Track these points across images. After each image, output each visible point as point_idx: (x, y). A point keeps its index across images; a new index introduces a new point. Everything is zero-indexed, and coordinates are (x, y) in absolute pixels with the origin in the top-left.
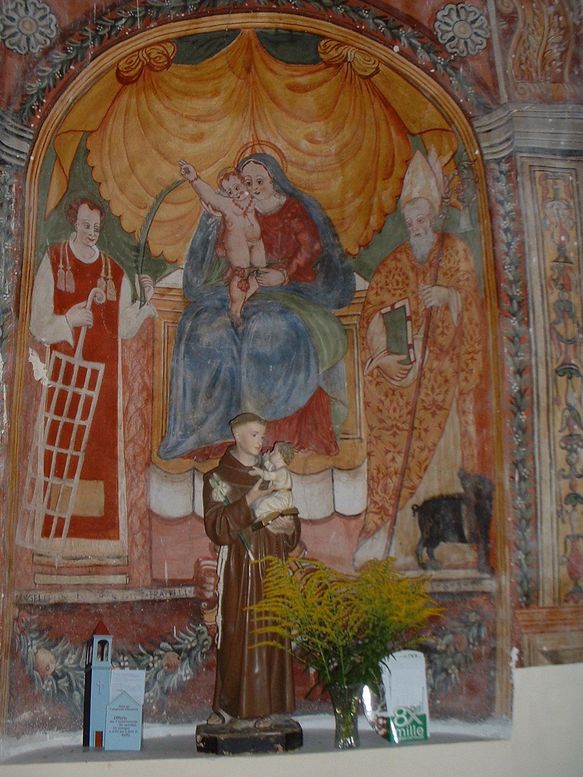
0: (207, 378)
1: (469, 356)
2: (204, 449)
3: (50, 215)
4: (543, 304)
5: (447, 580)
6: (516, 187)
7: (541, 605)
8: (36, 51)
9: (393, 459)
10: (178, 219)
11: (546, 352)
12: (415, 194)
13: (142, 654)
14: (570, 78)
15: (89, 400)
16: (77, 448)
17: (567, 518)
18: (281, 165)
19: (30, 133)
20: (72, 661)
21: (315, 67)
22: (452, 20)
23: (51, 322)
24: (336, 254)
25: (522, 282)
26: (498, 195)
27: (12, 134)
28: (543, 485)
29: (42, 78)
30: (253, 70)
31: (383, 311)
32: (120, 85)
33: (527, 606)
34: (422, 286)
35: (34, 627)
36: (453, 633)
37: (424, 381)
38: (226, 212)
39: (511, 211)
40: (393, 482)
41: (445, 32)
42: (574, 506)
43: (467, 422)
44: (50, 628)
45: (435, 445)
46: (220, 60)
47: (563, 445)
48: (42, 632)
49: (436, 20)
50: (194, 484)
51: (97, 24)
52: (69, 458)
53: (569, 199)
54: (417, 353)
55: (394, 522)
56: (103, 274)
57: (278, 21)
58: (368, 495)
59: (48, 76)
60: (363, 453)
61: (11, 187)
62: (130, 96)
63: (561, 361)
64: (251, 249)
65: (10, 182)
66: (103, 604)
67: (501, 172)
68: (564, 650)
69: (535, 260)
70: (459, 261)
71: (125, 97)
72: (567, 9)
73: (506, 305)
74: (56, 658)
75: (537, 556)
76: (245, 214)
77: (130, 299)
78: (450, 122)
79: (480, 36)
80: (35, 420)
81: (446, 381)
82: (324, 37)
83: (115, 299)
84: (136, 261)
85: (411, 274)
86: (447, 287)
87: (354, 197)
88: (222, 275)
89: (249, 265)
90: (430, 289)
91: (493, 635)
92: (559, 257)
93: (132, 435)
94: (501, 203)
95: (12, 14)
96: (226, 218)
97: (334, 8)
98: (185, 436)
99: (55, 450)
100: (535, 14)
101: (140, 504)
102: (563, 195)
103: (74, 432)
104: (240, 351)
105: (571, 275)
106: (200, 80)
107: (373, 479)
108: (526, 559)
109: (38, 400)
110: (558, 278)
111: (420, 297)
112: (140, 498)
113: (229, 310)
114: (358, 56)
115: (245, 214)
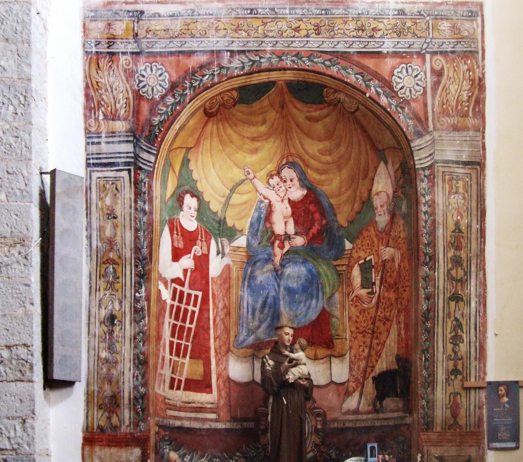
0: (260, 301)
1: (402, 289)
2: (259, 343)
3: (168, 201)
4: (444, 259)
5: (389, 419)
6: (433, 186)
7: (435, 430)
8: (157, 97)
9: (363, 351)
10: (242, 204)
11: (444, 287)
12: (380, 189)
13: (226, 458)
14: (473, 114)
15: (193, 312)
16: (187, 341)
17: (451, 383)
18: (304, 169)
19: (155, 150)
20: (188, 460)
21: (322, 106)
22: (403, 74)
23: (171, 266)
24: (336, 225)
25: (432, 244)
26: (422, 190)
27: (145, 150)
28: (439, 364)
29: (161, 115)
30: (285, 108)
31: (360, 262)
32: (206, 118)
33: (427, 430)
34: (381, 247)
35: (167, 438)
36: (391, 448)
37: (381, 304)
38: (271, 199)
39: (429, 200)
40: (362, 364)
41: (398, 83)
42: (456, 376)
43: (400, 328)
44: (176, 440)
45: (385, 342)
46: (265, 101)
47: (451, 341)
48: (171, 442)
49: (393, 75)
50: (253, 364)
51: (192, 79)
52: (183, 346)
53: (465, 193)
54: (376, 289)
55: (363, 387)
56: (199, 238)
57: (298, 76)
58: (350, 371)
59: (164, 113)
60: (347, 347)
61: (145, 183)
62: (213, 125)
63: (452, 292)
64: (286, 223)
65: (145, 180)
66: (204, 429)
67: (425, 176)
68: (446, 456)
69: (441, 231)
70: (400, 232)
71: (210, 125)
72: (475, 67)
73: (422, 258)
74: (180, 457)
75: (434, 403)
76: (282, 201)
77: (215, 253)
78: (399, 143)
79: (419, 85)
80: (163, 323)
81: (391, 304)
82: (326, 87)
83: (207, 253)
84: (219, 230)
85: (375, 240)
86: (393, 248)
87: (347, 190)
88: (269, 239)
89: (284, 233)
90: (384, 249)
91: (410, 447)
92: (456, 229)
93: (218, 334)
94: (424, 196)
95: (143, 73)
96: (272, 203)
97: (332, 67)
98: (248, 336)
99: (175, 341)
100: (455, 70)
101: (224, 374)
102: (461, 190)
103: (186, 330)
104: (279, 286)
105: (462, 240)
106: (253, 114)
107: (352, 362)
108: (427, 405)
109: (165, 311)
110: (454, 242)
111: (380, 254)
112: (223, 371)
113: (273, 260)
114: (347, 99)
115: (282, 201)
